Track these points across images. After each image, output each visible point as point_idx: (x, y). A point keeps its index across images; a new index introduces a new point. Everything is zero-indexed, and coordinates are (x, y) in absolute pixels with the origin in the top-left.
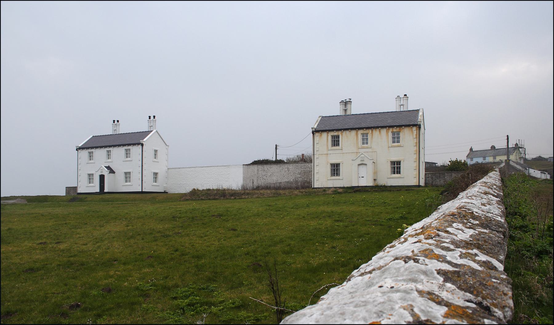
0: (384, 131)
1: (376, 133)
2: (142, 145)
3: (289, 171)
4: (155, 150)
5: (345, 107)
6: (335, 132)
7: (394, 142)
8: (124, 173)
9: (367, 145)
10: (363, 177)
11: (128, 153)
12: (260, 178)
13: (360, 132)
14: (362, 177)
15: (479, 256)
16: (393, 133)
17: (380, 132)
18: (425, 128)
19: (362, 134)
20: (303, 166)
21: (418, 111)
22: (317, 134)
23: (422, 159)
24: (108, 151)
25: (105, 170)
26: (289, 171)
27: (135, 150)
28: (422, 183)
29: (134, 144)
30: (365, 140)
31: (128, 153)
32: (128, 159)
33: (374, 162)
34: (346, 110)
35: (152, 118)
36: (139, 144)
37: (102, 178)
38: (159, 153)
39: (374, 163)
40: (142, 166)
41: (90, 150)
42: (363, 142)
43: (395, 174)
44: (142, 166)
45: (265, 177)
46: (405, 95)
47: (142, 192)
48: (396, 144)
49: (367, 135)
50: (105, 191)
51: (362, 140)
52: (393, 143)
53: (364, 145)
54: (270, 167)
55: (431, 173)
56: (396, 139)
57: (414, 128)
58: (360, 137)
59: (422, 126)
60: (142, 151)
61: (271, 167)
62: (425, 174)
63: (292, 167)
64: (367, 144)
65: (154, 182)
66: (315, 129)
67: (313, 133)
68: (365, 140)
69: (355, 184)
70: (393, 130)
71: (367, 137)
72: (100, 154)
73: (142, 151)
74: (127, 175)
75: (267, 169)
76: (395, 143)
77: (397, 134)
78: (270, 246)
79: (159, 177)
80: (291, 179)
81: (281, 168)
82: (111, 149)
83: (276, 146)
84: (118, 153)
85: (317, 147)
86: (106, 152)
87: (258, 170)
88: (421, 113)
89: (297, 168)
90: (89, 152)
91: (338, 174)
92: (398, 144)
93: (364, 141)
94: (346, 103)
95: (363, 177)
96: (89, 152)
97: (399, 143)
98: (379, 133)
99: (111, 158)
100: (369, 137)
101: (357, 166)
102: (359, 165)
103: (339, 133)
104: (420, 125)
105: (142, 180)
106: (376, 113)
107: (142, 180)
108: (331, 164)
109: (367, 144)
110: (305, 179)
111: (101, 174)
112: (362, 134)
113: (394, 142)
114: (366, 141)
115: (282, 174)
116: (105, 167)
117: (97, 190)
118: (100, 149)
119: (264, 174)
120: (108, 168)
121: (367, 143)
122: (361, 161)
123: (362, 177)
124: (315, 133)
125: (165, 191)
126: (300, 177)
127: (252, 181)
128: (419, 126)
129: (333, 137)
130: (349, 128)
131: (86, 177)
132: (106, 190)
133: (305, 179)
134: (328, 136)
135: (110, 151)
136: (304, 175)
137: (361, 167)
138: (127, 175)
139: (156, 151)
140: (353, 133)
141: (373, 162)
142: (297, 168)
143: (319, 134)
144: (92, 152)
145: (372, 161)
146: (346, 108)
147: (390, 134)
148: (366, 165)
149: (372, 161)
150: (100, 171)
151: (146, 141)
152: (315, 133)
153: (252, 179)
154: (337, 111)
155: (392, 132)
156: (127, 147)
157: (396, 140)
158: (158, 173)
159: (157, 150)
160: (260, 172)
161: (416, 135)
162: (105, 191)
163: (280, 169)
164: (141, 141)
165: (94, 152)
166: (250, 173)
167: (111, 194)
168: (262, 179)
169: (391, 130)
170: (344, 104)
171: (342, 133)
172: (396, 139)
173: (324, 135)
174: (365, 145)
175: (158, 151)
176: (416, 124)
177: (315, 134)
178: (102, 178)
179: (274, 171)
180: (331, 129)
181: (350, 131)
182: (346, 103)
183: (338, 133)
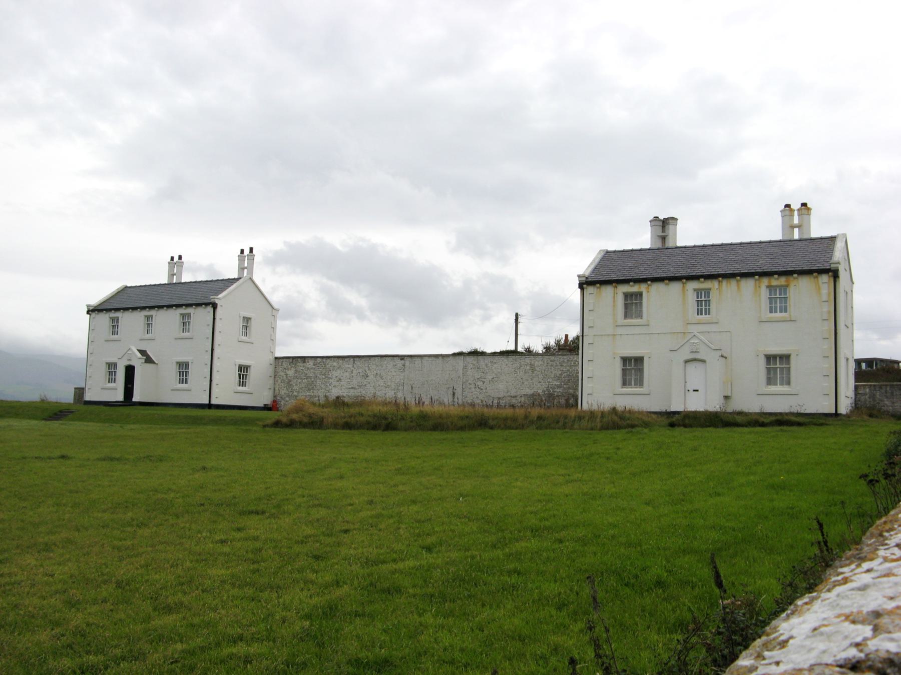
0: (748, 285)
1: (729, 288)
2: (215, 306)
3: (535, 372)
4: (243, 317)
5: (663, 232)
6: (631, 286)
7: (699, 312)
8: (175, 364)
9: (707, 316)
10: (697, 391)
11: (185, 323)
12: (470, 384)
13: (692, 285)
14: (694, 391)
15: (855, 581)
16: (698, 292)
17: (738, 286)
18: (854, 280)
19: (695, 290)
20: (566, 360)
21: (833, 239)
22: (590, 290)
23: (843, 352)
24: (148, 318)
25: (136, 356)
26: (533, 370)
27: (202, 316)
28: (845, 407)
29: (198, 305)
30: (703, 304)
31: (185, 323)
32: (186, 334)
33: (725, 355)
34: (664, 239)
35: (176, 259)
36: (207, 304)
37: (130, 371)
38: (254, 324)
39: (726, 358)
40: (212, 350)
41: (113, 314)
42: (698, 309)
43: (777, 385)
44: (212, 350)
45: (480, 383)
46: (804, 205)
47: (210, 406)
48: (778, 315)
49: (709, 293)
50: (134, 400)
51: (696, 303)
52: (771, 312)
53: (700, 316)
54: (491, 362)
55: (871, 386)
56: (778, 302)
57: (824, 278)
58: (691, 297)
59: (842, 274)
60: (214, 319)
61: (495, 361)
62: (856, 387)
63: (541, 363)
64: (709, 314)
65: (179, 383)
66: (587, 278)
67: (581, 286)
68: (703, 304)
69: (677, 406)
70: (770, 282)
71: (709, 297)
72: (131, 322)
73: (214, 319)
74: (183, 369)
75: (486, 365)
76: (776, 312)
77: (780, 290)
78: (800, 624)
79: (253, 374)
80: (539, 388)
81: (517, 365)
82: (153, 312)
83: (517, 315)
84: (166, 321)
85: (590, 318)
86: (143, 318)
87: (465, 367)
88: (839, 245)
89: (552, 365)
90: (111, 318)
91: (640, 382)
92: (783, 314)
93: (702, 306)
94: (664, 225)
95: (697, 391)
96: (111, 318)
97: (786, 311)
98: (736, 288)
99: (191, 330)
100: (714, 297)
101: (683, 364)
102: (686, 362)
103: (642, 288)
104: (838, 270)
105: (211, 381)
106: (731, 244)
107: (211, 381)
108: (622, 358)
109: (709, 314)
110: (571, 391)
111: (128, 363)
112: (695, 290)
113: (699, 312)
114: (706, 306)
115: (518, 377)
116: (138, 350)
117: (120, 397)
118: (131, 312)
119: (479, 377)
120: (143, 353)
121: (708, 312)
122: (692, 352)
123: (694, 391)
124: (585, 286)
125: (265, 405)
126: (559, 387)
127: (450, 392)
128: (835, 274)
129: (627, 296)
130: (665, 276)
131: (104, 369)
132: (136, 398)
133: (571, 391)
134: (615, 293)
135: (152, 316)
136: (569, 380)
137: (691, 367)
138: (183, 369)
139: (247, 320)
140: (676, 287)
141: (722, 356)
142: (552, 365)
143: (595, 289)
144: (189, 315)
145: (719, 353)
146: (663, 234)
147: (764, 293)
148: (704, 361)
149: (719, 353)
150: (125, 358)
151: (224, 297)
152: (585, 286)
153: (452, 386)
154: (643, 239)
155: (767, 287)
156: (185, 309)
157: (704, 307)
158: (249, 366)
159: (250, 319)
160: (469, 372)
161: (829, 294)
162: (134, 400)
163: (515, 366)
164: (212, 297)
165: (154, 316)
166: (448, 372)
167: (147, 407)
168: (472, 386)
169: (765, 281)
170: (661, 224)
171: (648, 288)
172: (778, 302)
173: (608, 291)
174: (704, 316)
175: (252, 320)
176: (828, 268)
177: (585, 290)
178: (130, 371)
179: (499, 370)
180: (623, 278)
181: (667, 284)
182: (664, 225)
183: (640, 288)
